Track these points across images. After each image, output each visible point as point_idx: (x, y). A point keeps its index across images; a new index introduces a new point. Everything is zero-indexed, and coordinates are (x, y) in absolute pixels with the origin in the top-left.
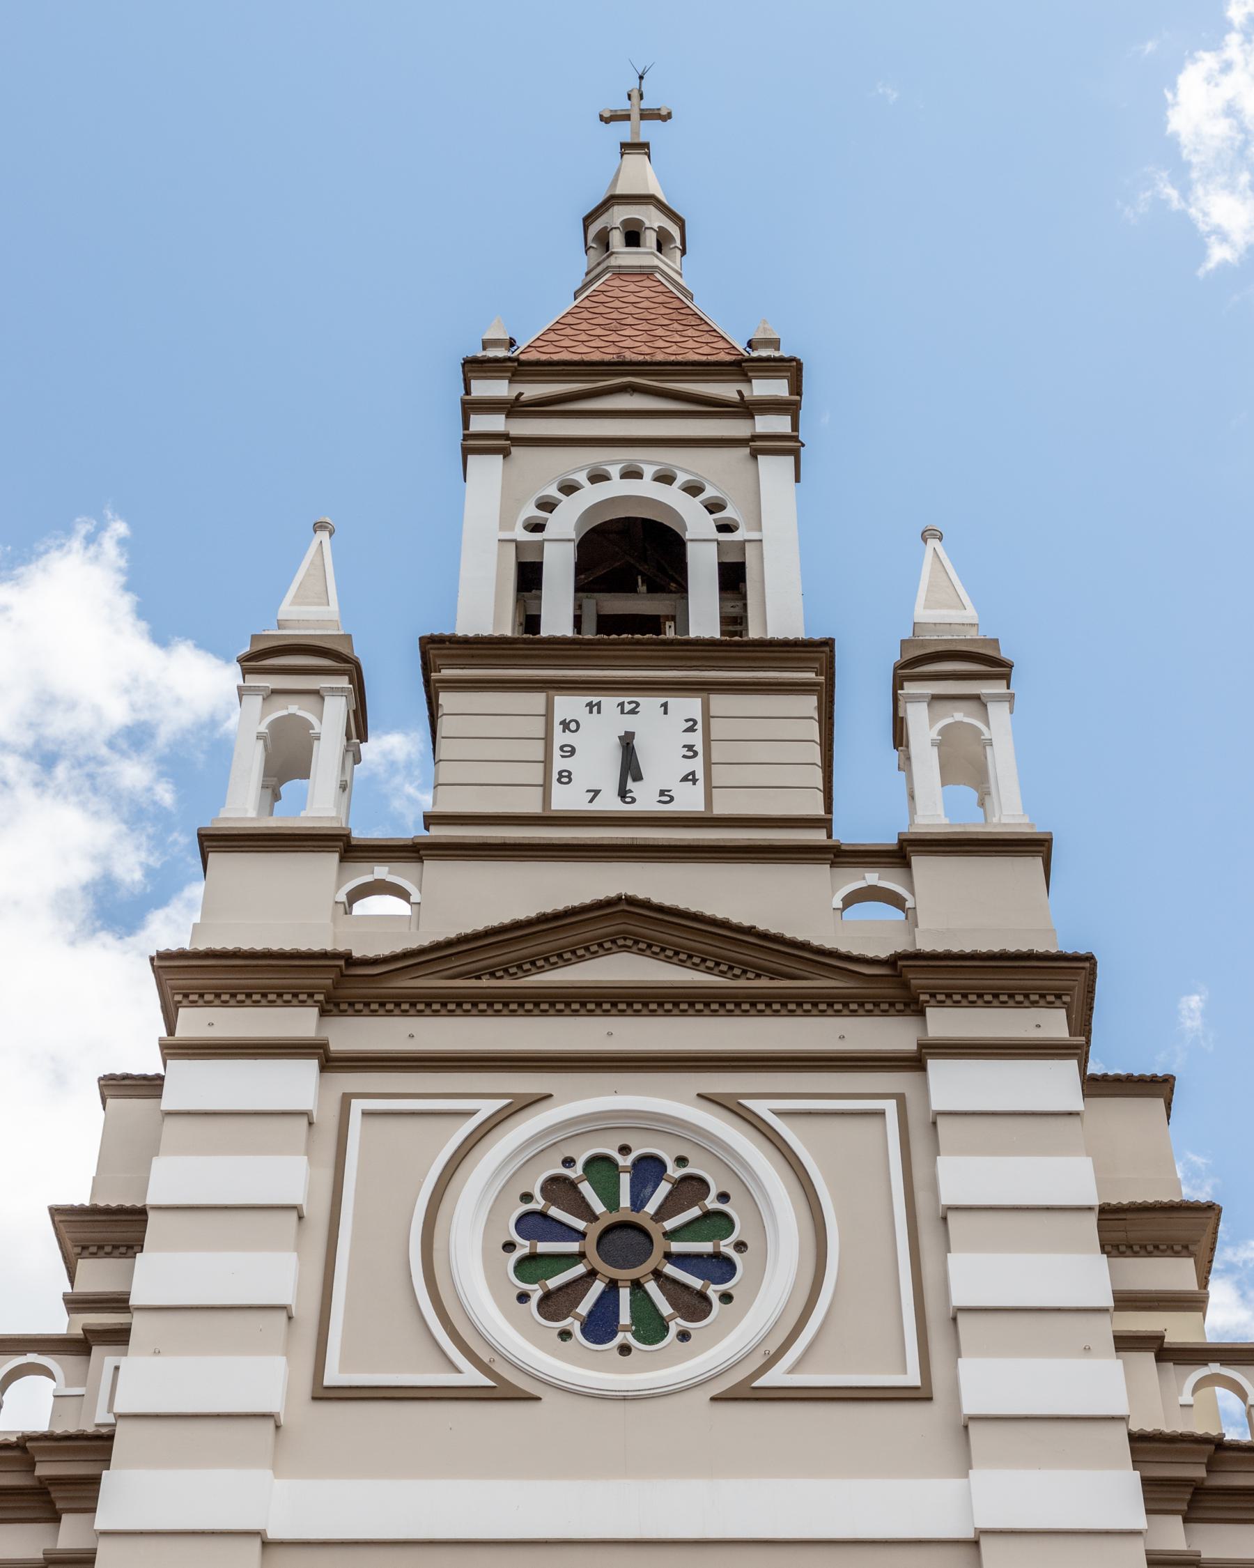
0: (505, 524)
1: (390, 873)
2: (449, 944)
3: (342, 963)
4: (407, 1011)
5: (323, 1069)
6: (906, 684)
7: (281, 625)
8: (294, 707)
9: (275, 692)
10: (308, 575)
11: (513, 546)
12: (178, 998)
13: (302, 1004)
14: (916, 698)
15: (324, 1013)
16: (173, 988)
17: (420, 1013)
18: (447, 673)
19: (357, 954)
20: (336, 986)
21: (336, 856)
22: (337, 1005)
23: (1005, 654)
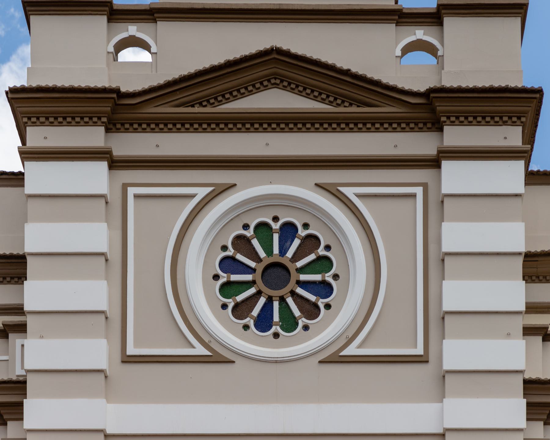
1: (138, 31)
3: (114, 96)
12: (25, 120)
13: (95, 124)
15: (108, 130)
16: (21, 113)
19: (123, 90)
20: (114, 111)
21: (105, 18)
22: (115, 125)
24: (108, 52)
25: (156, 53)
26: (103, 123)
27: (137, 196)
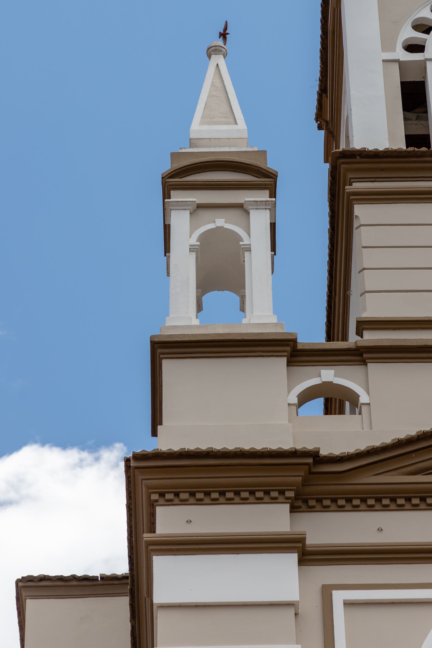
0: (387, 45)
1: (335, 376)
2: (410, 441)
3: (310, 460)
4: (358, 506)
5: (301, 562)
6: (173, 193)
7: (192, 143)
8: (221, 221)
9: (200, 207)
10: (210, 96)
11: (397, 65)
12: (154, 497)
13: (274, 500)
14: (181, 205)
15: (293, 509)
16: (148, 488)
17: (386, 508)
18: (358, 186)
19: (324, 452)
20: (305, 483)
21: (284, 360)
22: (306, 501)
23: (271, 164)
24: (289, 404)
25: (369, 404)
26: (287, 498)
27: (348, 604)
